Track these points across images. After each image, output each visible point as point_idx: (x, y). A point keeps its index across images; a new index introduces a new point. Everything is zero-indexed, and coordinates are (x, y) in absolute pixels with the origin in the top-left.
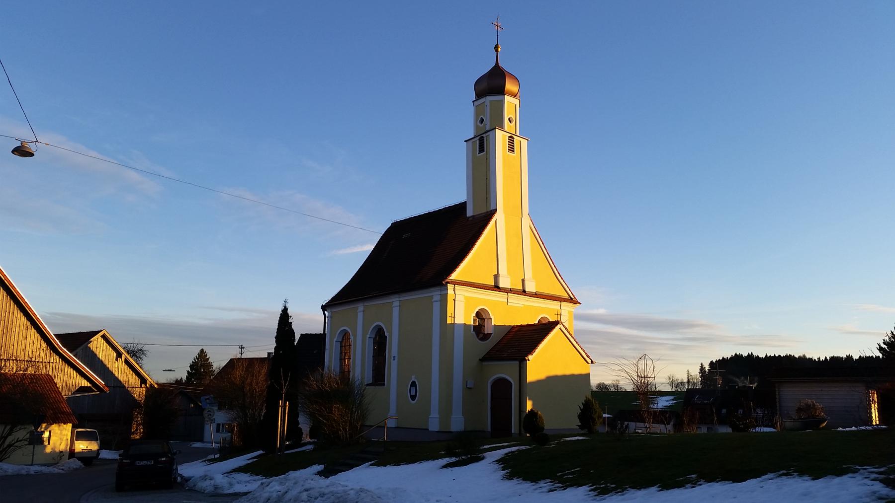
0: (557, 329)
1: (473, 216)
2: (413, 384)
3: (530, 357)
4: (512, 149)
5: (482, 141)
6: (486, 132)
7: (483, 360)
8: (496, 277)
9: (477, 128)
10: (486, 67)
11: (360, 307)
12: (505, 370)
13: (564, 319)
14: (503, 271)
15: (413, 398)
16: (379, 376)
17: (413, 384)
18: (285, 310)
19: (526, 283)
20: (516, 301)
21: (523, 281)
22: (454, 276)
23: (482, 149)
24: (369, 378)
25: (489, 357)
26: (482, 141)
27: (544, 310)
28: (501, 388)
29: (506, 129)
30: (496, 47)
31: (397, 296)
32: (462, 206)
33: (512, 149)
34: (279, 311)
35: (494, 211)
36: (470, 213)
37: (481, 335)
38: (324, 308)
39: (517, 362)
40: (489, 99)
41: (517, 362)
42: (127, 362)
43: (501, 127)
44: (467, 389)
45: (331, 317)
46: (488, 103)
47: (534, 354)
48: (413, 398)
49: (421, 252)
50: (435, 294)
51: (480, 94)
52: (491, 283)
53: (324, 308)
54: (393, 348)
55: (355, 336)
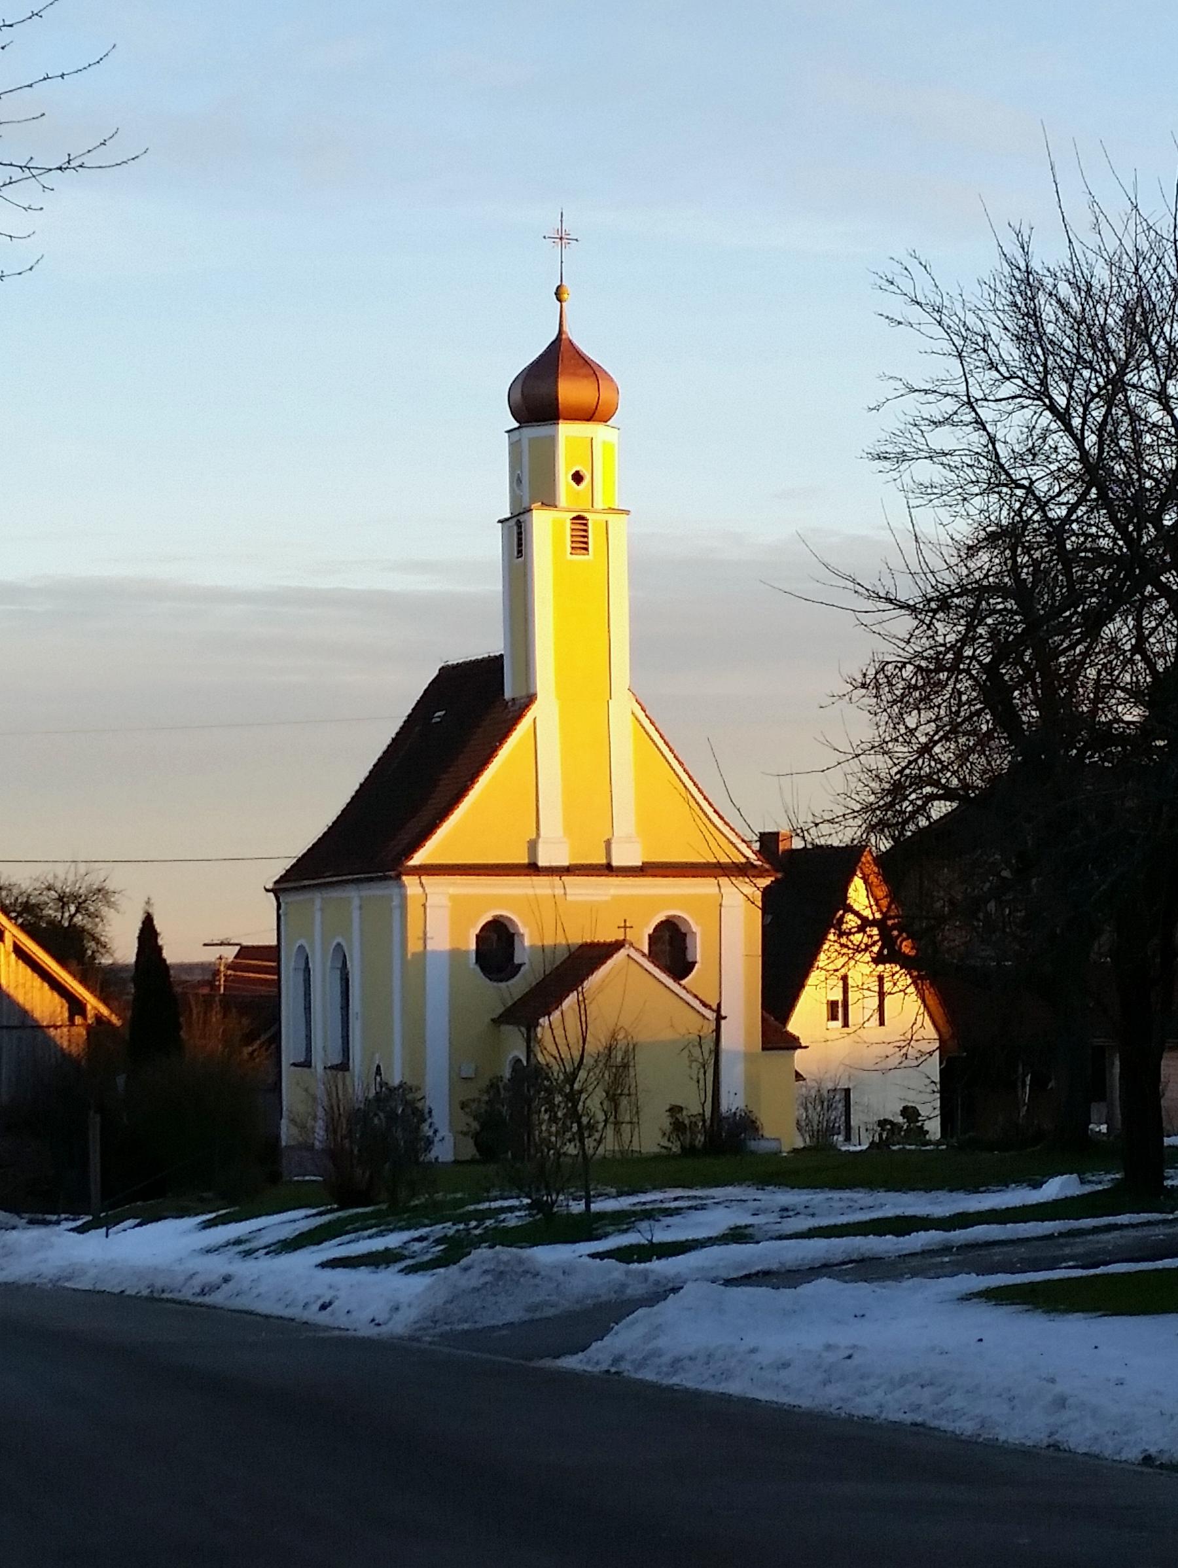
4: (581, 544)
5: (519, 524)
8: (533, 846)
18: (148, 921)
20: (581, 890)
21: (608, 844)
22: (418, 859)
26: (519, 524)
30: (559, 294)
33: (581, 544)
42: (19, 951)
43: (550, 503)
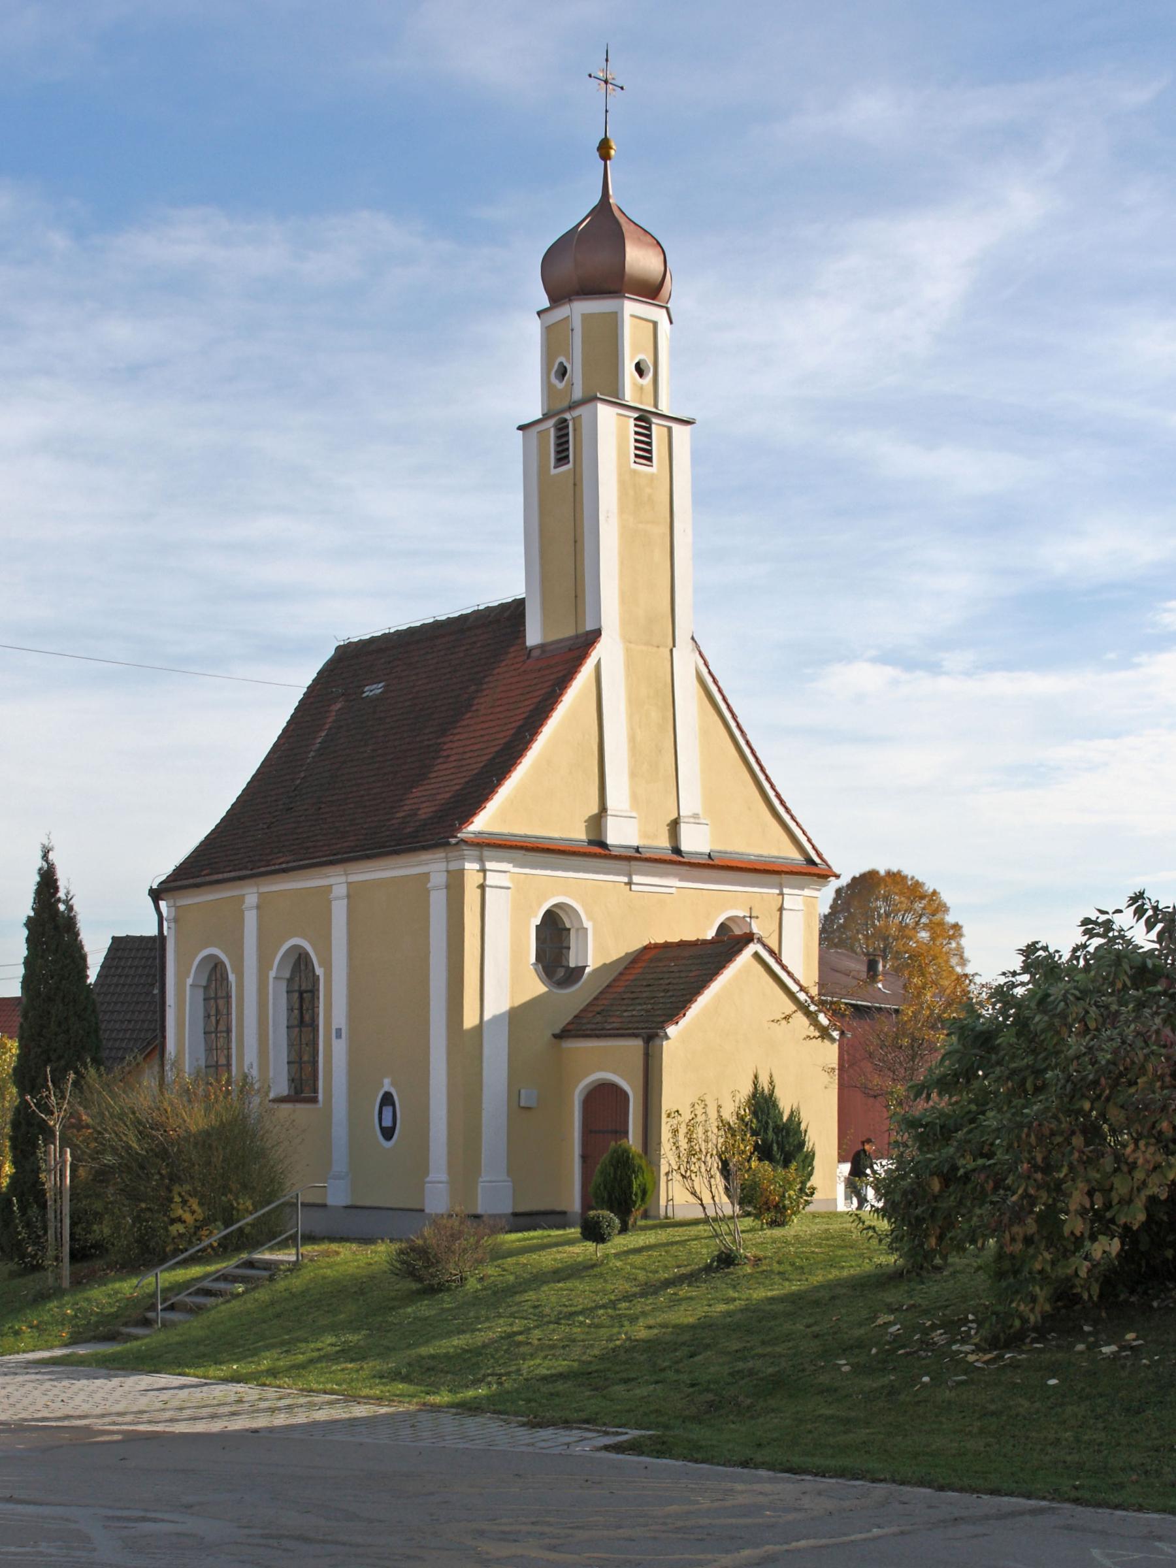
0: (745, 956)
1: (542, 647)
2: (387, 1099)
3: (671, 1030)
4: (645, 454)
5: (562, 429)
6: (572, 407)
7: (563, 1035)
8: (598, 821)
9: (549, 392)
10: (574, 212)
11: (250, 895)
12: (608, 1062)
13: (755, 930)
14: (617, 799)
15: (388, 1133)
16: (304, 1086)
17: (387, 1099)
19: (685, 830)
23: (562, 457)
24: (281, 1087)
25: (582, 1026)
26: (562, 429)
27: (685, 912)
28: (605, 1105)
29: (629, 397)
31: (338, 869)
32: (514, 613)
34: (23, 904)
35: (596, 634)
36: (534, 636)
37: (561, 973)
38: (156, 895)
39: (638, 1043)
40: (581, 308)
41: (638, 1043)
44: (519, 1110)
45: (176, 920)
46: (577, 324)
47: (683, 1022)
48: (388, 1133)
49: (401, 742)
50: (432, 867)
51: (560, 292)
52: (579, 833)
53: (156, 895)
54: (335, 1007)
55: (327, 964)
